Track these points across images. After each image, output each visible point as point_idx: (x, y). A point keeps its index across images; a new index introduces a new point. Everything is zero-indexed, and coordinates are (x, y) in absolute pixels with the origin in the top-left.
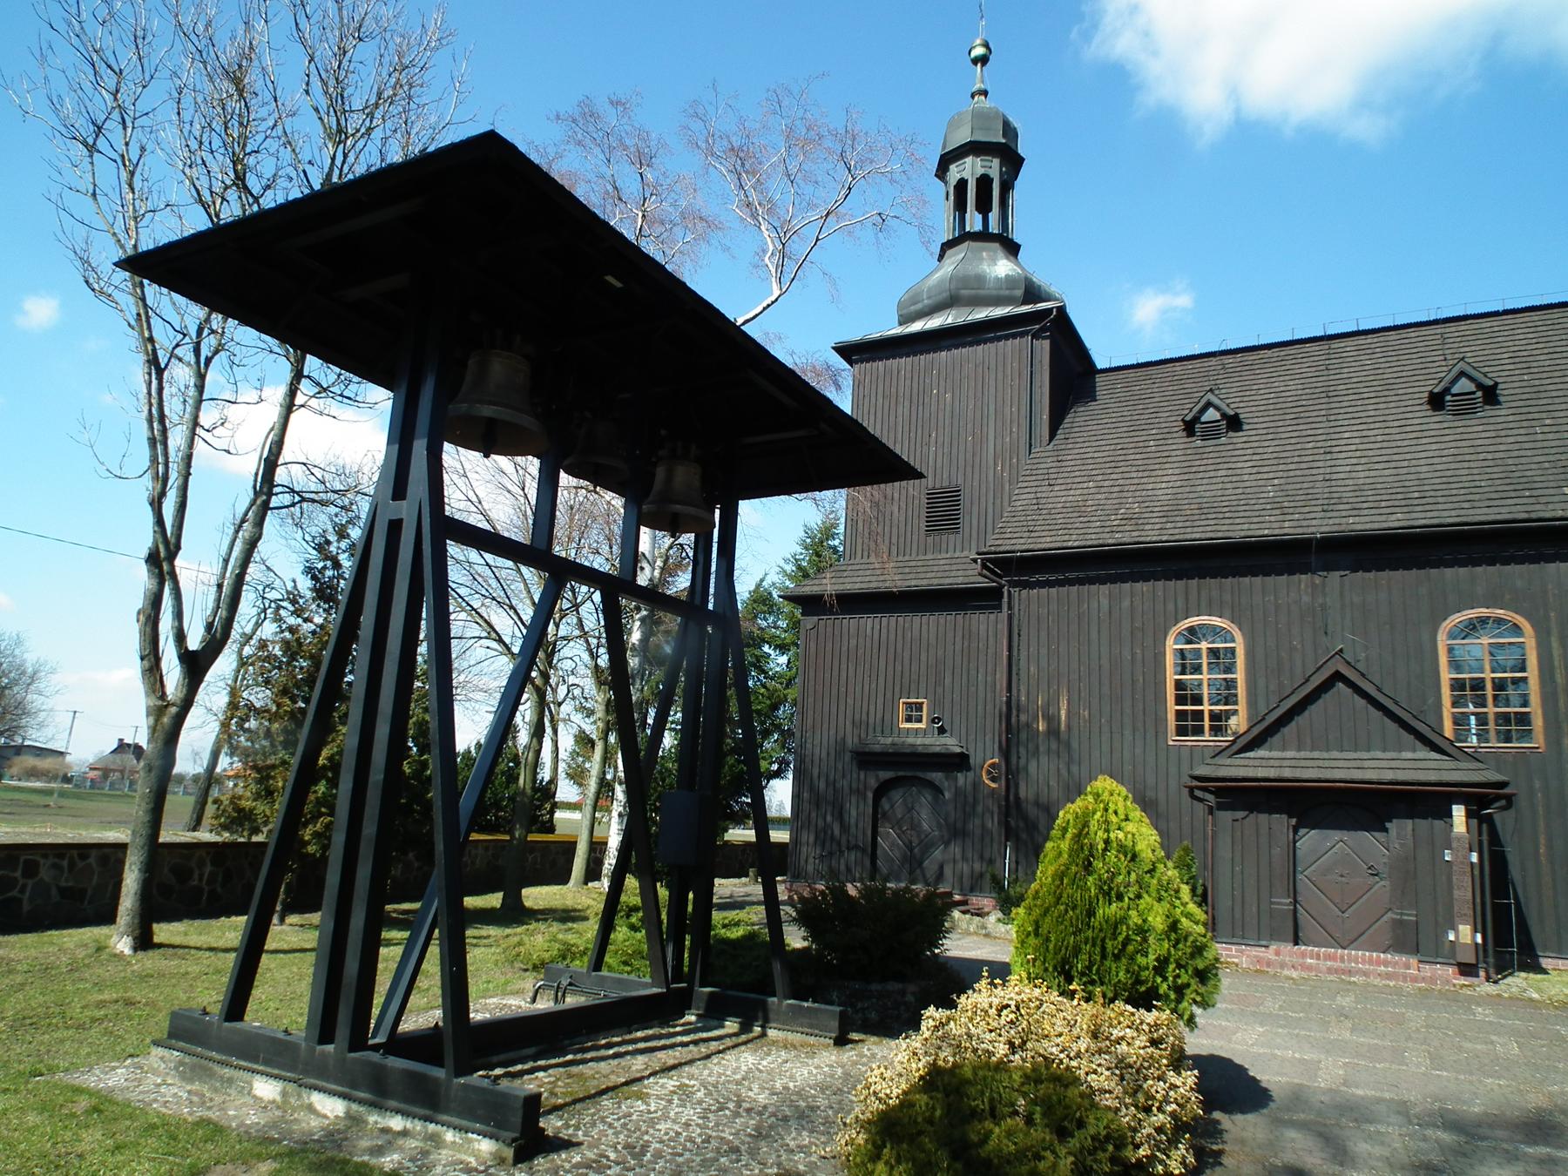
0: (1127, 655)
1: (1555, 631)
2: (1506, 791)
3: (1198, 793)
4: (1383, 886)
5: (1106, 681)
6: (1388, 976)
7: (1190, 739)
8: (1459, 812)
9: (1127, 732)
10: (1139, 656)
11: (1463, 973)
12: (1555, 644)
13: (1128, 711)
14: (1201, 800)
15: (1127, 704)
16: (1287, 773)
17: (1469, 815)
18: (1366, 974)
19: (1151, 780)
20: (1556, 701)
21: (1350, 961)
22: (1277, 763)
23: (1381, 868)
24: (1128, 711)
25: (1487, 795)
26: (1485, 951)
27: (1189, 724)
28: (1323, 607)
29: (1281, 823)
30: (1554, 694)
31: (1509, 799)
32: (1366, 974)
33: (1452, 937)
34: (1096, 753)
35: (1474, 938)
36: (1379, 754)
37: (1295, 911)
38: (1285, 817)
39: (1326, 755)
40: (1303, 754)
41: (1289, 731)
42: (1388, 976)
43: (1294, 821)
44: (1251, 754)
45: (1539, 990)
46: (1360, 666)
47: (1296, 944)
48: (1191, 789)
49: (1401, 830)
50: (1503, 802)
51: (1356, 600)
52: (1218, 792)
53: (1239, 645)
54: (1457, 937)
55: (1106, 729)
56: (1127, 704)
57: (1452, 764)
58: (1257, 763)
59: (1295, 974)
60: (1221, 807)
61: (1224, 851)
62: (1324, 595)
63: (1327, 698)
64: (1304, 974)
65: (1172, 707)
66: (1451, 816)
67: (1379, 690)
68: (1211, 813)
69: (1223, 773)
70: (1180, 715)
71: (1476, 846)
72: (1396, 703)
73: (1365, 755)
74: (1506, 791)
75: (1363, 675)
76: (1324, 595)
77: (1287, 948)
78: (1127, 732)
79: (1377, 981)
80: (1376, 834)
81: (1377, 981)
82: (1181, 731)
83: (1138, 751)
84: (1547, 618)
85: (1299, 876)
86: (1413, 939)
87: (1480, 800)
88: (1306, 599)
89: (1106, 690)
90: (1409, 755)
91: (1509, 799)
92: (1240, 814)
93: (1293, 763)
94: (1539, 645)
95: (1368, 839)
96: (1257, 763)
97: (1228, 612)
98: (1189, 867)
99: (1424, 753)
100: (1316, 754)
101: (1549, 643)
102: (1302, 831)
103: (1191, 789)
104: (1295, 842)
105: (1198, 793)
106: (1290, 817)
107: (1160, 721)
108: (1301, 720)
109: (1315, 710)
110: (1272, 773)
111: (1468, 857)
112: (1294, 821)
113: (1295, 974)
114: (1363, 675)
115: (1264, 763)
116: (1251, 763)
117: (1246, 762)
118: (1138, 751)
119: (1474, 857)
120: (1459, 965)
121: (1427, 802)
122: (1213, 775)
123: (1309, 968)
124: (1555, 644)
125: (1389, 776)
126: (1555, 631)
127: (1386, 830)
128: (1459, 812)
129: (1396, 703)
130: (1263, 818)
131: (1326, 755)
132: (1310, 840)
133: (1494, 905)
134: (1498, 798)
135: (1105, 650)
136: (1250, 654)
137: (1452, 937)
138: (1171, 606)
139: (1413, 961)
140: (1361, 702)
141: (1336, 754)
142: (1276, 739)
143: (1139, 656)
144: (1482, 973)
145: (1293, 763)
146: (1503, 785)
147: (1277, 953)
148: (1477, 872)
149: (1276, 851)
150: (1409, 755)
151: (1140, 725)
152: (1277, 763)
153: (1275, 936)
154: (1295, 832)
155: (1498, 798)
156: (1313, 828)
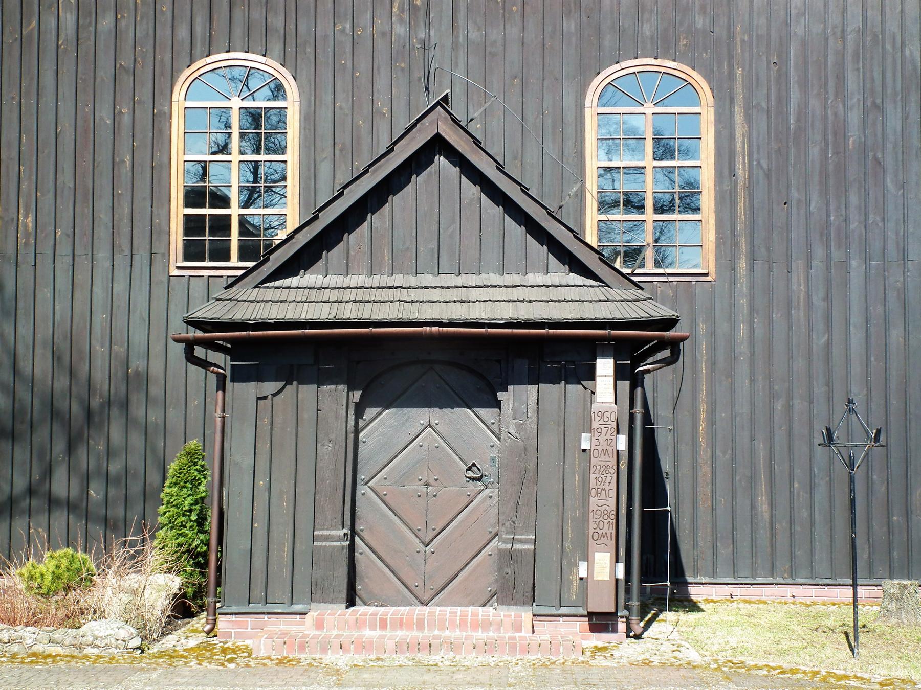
0: (105, 114)
1: (739, 98)
2: (672, 333)
3: (199, 352)
4: (488, 499)
5: (66, 164)
6: (487, 647)
7: (207, 268)
8: (605, 367)
9: (102, 254)
10: (126, 119)
11: (594, 628)
12: (739, 118)
13: (104, 216)
14: (204, 364)
15: (103, 205)
16: (349, 312)
17: (619, 374)
18: (453, 647)
19: (139, 337)
20: (734, 204)
21: (431, 626)
22: (334, 295)
23: (486, 468)
24: (104, 216)
25: (648, 340)
26: (628, 591)
27: (205, 238)
28: (426, 46)
29: (335, 398)
30: (733, 193)
31: (674, 345)
32: (453, 647)
33: (583, 571)
34: (45, 293)
35: (614, 571)
36: (495, 279)
37: (352, 548)
38: (342, 388)
39: (412, 281)
40: (376, 280)
41: (357, 239)
42: (487, 647)
43: (357, 395)
44: (294, 281)
45: (697, 644)
46: (476, 129)
47: (351, 603)
48: (190, 345)
49: (520, 400)
50: (666, 353)
51: (474, 35)
52: (236, 349)
53: (292, 104)
54: (590, 570)
55: (64, 249)
56: (103, 205)
57: (600, 293)
58: (301, 295)
59: (341, 660)
60: (239, 375)
61: (240, 455)
62: (428, 24)
63: (421, 180)
64: (359, 659)
65: (178, 211)
66: (591, 376)
67: (500, 168)
68: (222, 386)
69: (242, 313)
70: (193, 225)
71: (625, 426)
72: (525, 190)
73: (473, 280)
74: (672, 333)
75: (477, 142)
76: (428, 24)
77: (335, 614)
78: (102, 254)
79: (470, 659)
80: (482, 412)
81: (470, 659)
82: (192, 252)
83: (120, 287)
84: (731, 76)
85: (361, 489)
86: (522, 583)
87: (640, 347)
88: (400, 30)
89: (66, 178)
90: (539, 279)
91: (674, 345)
92: (270, 387)
93: (360, 294)
94: (719, 119)
95: (464, 419)
96: (301, 295)
97: (276, 47)
98: (195, 483)
99: (561, 275)
100: (398, 280)
101: (732, 114)
102: (370, 412)
103: (190, 345)
104: (357, 432)
105: (199, 352)
106: (351, 388)
107: (157, 233)
108: (377, 221)
109: (400, 201)
110: (323, 313)
111: (611, 442)
112: (357, 395)
113: (341, 660)
114: (477, 142)
115: (313, 295)
116: (292, 295)
117: (284, 294)
118: (120, 287)
119: (622, 443)
120: (591, 615)
121: (551, 355)
122: (226, 318)
123: (363, 646)
124: (739, 118)
125: (506, 313)
126: (739, 98)
127: (497, 404)
128: (605, 367)
129: (525, 190)
130: (308, 391)
131: (412, 281)
132: (386, 426)
133: (643, 514)
134: (662, 344)
135: (66, 108)
136: (310, 121)
137: (583, 571)
138: (183, 32)
139: (525, 614)
140: (471, 190)
141: (428, 279)
142: (336, 254)
143: (126, 119)
144: (622, 626)
145: (360, 294)
146: (670, 323)
147: (319, 625)
148: (624, 466)
149: (326, 449)
150: (539, 279)
151: (124, 243)
152: (334, 295)
153: (318, 593)
154: (359, 414)
155: (662, 344)
156: (387, 407)
